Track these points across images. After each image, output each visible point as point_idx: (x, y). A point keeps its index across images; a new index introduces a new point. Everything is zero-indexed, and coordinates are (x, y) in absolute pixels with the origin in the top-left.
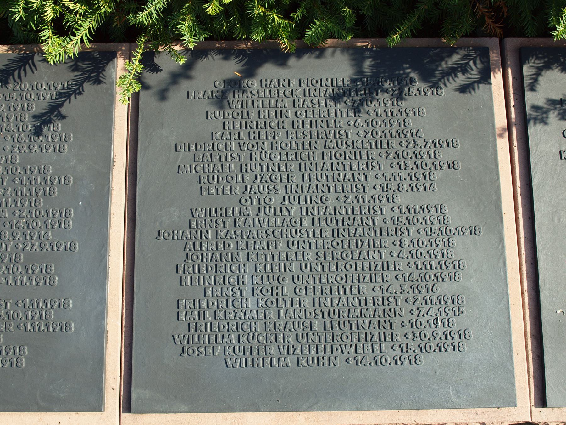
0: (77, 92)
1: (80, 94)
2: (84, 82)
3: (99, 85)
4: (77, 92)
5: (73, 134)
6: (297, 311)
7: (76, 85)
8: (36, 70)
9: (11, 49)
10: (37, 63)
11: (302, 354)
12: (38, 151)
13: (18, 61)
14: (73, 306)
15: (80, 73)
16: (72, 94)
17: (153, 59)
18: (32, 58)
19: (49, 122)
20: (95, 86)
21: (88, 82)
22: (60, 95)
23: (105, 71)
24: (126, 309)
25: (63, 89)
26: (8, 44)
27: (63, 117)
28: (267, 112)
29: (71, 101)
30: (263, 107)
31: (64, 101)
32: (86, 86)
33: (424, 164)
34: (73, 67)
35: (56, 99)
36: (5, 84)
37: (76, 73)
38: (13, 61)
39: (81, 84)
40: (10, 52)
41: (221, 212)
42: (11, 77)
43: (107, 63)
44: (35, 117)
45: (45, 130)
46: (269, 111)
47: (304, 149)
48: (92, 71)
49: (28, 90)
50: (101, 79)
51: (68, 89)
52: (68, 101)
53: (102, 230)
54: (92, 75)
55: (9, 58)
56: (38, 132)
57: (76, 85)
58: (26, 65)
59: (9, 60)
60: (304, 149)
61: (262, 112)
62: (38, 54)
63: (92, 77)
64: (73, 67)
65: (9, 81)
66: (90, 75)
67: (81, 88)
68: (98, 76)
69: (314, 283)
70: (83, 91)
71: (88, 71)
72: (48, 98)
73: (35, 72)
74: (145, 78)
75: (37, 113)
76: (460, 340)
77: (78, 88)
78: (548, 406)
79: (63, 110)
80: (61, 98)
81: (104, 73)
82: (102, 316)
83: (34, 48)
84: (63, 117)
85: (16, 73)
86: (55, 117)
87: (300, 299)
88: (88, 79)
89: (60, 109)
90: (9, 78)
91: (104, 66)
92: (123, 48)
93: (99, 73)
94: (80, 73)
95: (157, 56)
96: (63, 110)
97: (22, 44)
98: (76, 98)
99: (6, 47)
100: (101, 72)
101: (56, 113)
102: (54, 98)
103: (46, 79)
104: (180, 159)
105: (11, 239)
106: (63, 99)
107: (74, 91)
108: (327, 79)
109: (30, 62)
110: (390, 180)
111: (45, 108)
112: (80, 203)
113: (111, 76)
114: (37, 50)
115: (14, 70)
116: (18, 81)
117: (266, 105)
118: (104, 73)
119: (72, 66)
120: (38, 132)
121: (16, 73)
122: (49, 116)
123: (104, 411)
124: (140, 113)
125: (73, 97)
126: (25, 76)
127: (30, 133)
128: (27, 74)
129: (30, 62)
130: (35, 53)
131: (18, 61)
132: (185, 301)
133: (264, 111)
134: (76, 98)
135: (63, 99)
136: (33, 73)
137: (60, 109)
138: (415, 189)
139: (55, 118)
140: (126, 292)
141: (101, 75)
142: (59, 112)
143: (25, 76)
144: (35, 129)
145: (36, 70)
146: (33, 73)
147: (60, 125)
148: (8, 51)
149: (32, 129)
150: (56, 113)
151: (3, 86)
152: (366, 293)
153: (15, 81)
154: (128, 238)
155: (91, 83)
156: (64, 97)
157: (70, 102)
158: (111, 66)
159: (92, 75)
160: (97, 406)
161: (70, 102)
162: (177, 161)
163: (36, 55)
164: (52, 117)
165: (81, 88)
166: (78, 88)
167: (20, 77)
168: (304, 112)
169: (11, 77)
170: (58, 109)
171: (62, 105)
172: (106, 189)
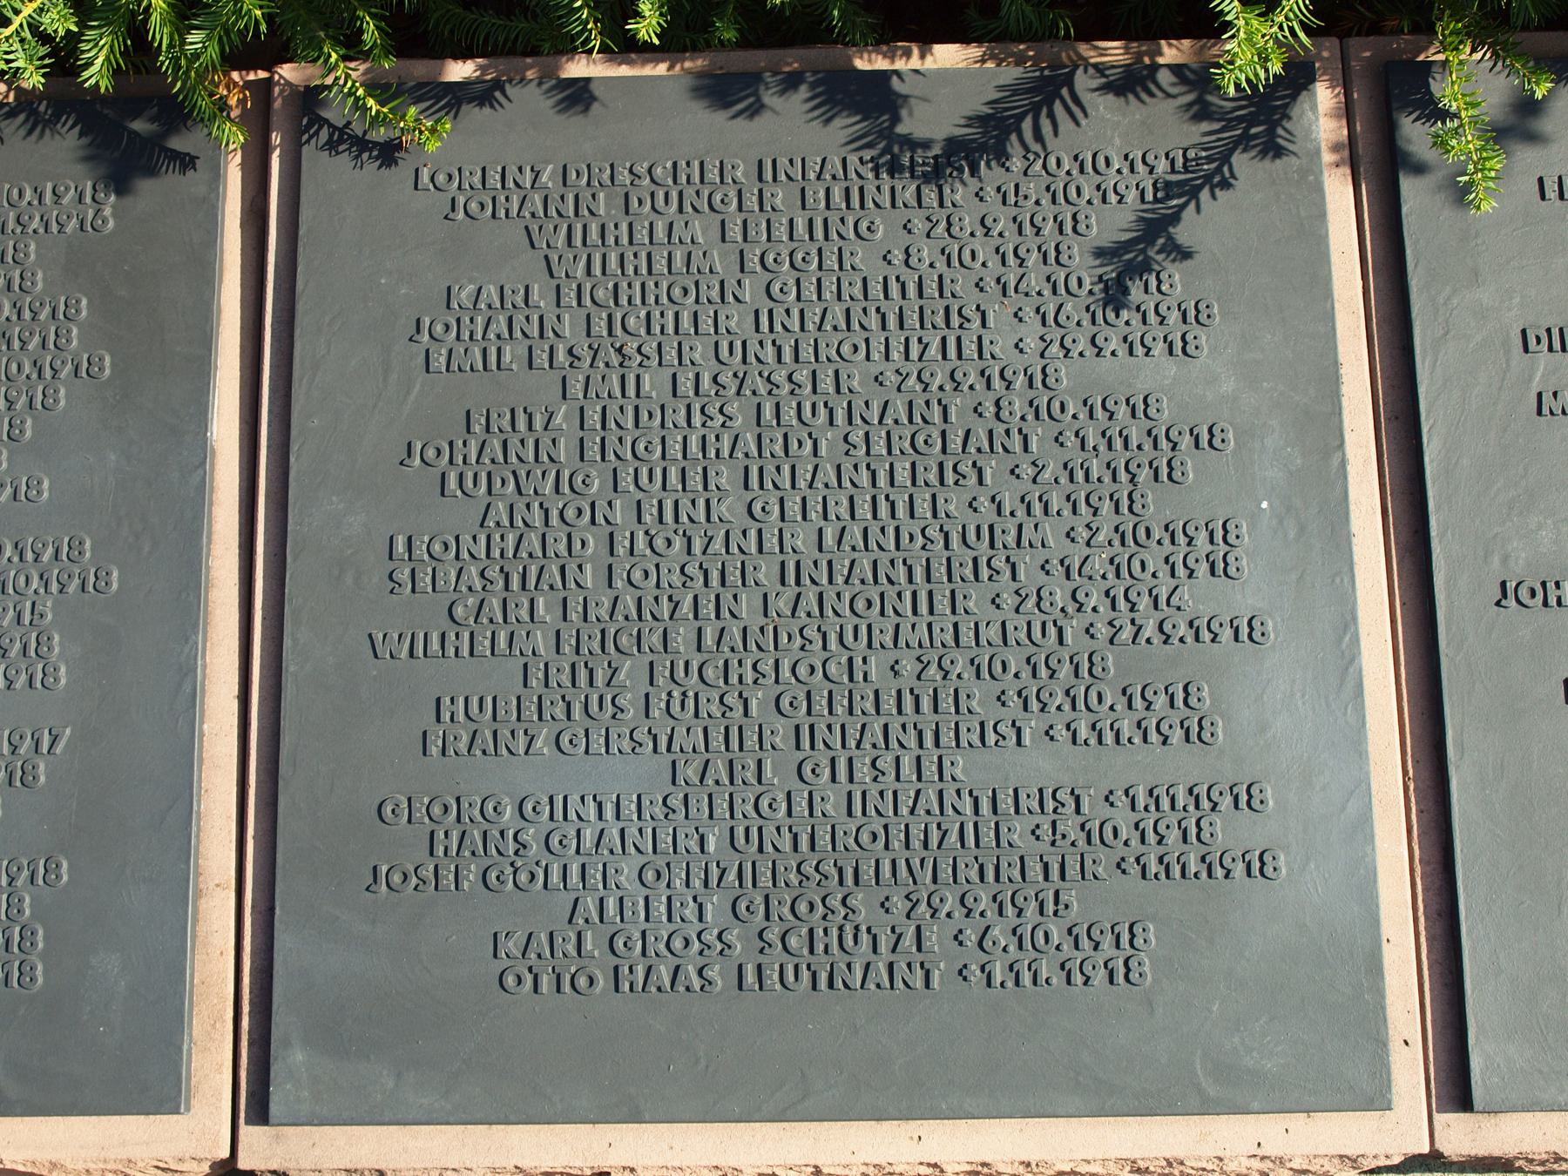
0: (1217, 179)
1: (1225, 185)
2: (1232, 151)
3: (1278, 161)
4: (1217, 179)
5: (1218, 300)
6: (632, 832)
7: (1209, 159)
8: (1086, 115)
9: (993, 57)
10: (1086, 98)
11: (919, 949)
12: (1120, 353)
13: (1028, 91)
14: (1276, 802)
15: (1216, 126)
16: (1200, 187)
17: (1428, 85)
18: (1069, 81)
19: (1145, 267)
20: (1267, 163)
21: (1244, 151)
22: (1168, 189)
23: (1289, 118)
24: (1420, 812)
25: (1173, 171)
26: (979, 41)
27: (1185, 254)
28: (643, 255)
29: (1202, 206)
30: (631, 242)
31: (1183, 207)
32: (1241, 161)
33: (1056, 405)
34: (1196, 108)
35: (1156, 200)
36: (998, 159)
37: (1205, 126)
38: (1014, 90)
39: (1225, 158)
40: (990, 65)
41: (503, 545)
42: (1014, 137)
43: (1294, 97)
44: (1100, 253)
45: (1136, 293)
46: (649, 255)
47: (797, 360)
48: (1251, 121)
49: (1068, 173)
50: (1280, 141)
51: (1187, 171)
52: (1192, 205)
53: (1338, 580)
54: (1253, 131)
55: (1002, 82)
56: (1114, 296)
57: (1209, 159)
58: (1053, 103)
59: (1000, 88)
60: (797, 360)
61: (629, 255)
62: (1086, 71)
63: (1256, 136)
64: (1196, 108)
65: (1009, 149)
66: (1246, 130)
67: (1226, 169)
68: (1271, 132)
69: (917, 711)
70: (1233, 176)
71: (1240, 119)
72: (1132, 196)
73: (1083, 122)
74: (1409, 141)
75: (1105, 243)
76: (1039, 919)
77: (1219, 170)
78: (271, 1120)
79: (1182, 233)
80: (1168, 197)
81: (1288, 125)
82: (1362, 827)
83: (1059, 53)
84: (1185, 254)
85: (1027, 125)
86: (1158, 252)
87: (810, 793)
88: (1244, 142)
89: (1171, 230)
90: (1008, 139)
91: (1286, 106)
92: (1325, 54)
93: (1272, 126)
94: (1216, 126)
95: (1438, 76)
96: (1182, 233)
97: (1022, 41)
98: (1214, 197)
99: (975, 51)
100: (1278, 123)
101: (1161, 241)
102: (1149, 197)
103: (1117, 141)
104: (1539, 374)
105: (1070, 610)
106: (1175, 202)
107: (1208, 178)
108: (520, 169)
109: (1065, 92)
110: (1139, 447)
111: (1126, 226)
112: (1264, 505)
113: (1308, 132)
114: (1069, 57)
115: (1020, 118)
116: (1037, 147)
117: (642, 235)
118: (1288, 125)
119: (1190, 105)
120: (1114, 296)
121: (1027, 125)
122: (1143, 251)
123: (188, 1109)
124: (300, 259)
125: (1205, 195)
126: (1056, 134)
127: (1091, 300)
128: (1061, 129)
129: (1065, 92)
130: (1077, 67)
131: (1028, 91)
132: (639, 797)
133: (635, 255)
134: (1214, 197)
135: (1175, 202)
136: (1078, 124)
137: (1171, 230)
138: (1206, 636)
139: (1160, 258)
140: (1416, 762)
141: (1280, 131)
142: (1170, 238)
143: (1056, 134)
144: (1106, 290)
145: (1086, 115)
146: (1078, 124)
147: (1175, 275)
148: (983, 61)
149: (1097, 289)
150: (1161, 241)
151: (993, 163)
152: (960, 776)
153: (1027, 150)
154: (1403, 604)
155: (1253, 153)
156: (1180, 196)
157: (1198, 210)
158: (1306, 106)
159: (1253, 131)
160: (160, 1092)
161: (1198, 210)
162: (1530, 380)
163: (1080, 71)
164: (1151, 253)
165: (1226, 169)
166: (1219, 170)
167: (1038, 137)
168: (814, 252)
169: (1014, 137)
170: (1166, 230)
171: (1175, 218)
172: (1335, 462)
